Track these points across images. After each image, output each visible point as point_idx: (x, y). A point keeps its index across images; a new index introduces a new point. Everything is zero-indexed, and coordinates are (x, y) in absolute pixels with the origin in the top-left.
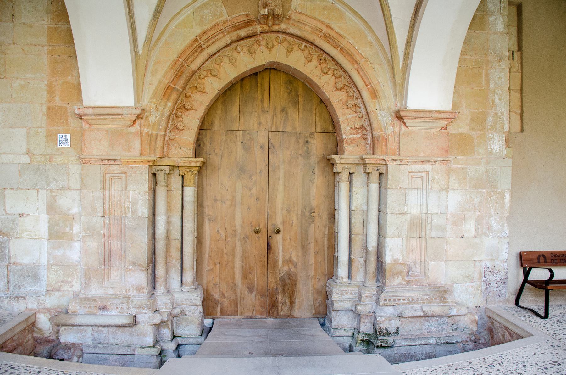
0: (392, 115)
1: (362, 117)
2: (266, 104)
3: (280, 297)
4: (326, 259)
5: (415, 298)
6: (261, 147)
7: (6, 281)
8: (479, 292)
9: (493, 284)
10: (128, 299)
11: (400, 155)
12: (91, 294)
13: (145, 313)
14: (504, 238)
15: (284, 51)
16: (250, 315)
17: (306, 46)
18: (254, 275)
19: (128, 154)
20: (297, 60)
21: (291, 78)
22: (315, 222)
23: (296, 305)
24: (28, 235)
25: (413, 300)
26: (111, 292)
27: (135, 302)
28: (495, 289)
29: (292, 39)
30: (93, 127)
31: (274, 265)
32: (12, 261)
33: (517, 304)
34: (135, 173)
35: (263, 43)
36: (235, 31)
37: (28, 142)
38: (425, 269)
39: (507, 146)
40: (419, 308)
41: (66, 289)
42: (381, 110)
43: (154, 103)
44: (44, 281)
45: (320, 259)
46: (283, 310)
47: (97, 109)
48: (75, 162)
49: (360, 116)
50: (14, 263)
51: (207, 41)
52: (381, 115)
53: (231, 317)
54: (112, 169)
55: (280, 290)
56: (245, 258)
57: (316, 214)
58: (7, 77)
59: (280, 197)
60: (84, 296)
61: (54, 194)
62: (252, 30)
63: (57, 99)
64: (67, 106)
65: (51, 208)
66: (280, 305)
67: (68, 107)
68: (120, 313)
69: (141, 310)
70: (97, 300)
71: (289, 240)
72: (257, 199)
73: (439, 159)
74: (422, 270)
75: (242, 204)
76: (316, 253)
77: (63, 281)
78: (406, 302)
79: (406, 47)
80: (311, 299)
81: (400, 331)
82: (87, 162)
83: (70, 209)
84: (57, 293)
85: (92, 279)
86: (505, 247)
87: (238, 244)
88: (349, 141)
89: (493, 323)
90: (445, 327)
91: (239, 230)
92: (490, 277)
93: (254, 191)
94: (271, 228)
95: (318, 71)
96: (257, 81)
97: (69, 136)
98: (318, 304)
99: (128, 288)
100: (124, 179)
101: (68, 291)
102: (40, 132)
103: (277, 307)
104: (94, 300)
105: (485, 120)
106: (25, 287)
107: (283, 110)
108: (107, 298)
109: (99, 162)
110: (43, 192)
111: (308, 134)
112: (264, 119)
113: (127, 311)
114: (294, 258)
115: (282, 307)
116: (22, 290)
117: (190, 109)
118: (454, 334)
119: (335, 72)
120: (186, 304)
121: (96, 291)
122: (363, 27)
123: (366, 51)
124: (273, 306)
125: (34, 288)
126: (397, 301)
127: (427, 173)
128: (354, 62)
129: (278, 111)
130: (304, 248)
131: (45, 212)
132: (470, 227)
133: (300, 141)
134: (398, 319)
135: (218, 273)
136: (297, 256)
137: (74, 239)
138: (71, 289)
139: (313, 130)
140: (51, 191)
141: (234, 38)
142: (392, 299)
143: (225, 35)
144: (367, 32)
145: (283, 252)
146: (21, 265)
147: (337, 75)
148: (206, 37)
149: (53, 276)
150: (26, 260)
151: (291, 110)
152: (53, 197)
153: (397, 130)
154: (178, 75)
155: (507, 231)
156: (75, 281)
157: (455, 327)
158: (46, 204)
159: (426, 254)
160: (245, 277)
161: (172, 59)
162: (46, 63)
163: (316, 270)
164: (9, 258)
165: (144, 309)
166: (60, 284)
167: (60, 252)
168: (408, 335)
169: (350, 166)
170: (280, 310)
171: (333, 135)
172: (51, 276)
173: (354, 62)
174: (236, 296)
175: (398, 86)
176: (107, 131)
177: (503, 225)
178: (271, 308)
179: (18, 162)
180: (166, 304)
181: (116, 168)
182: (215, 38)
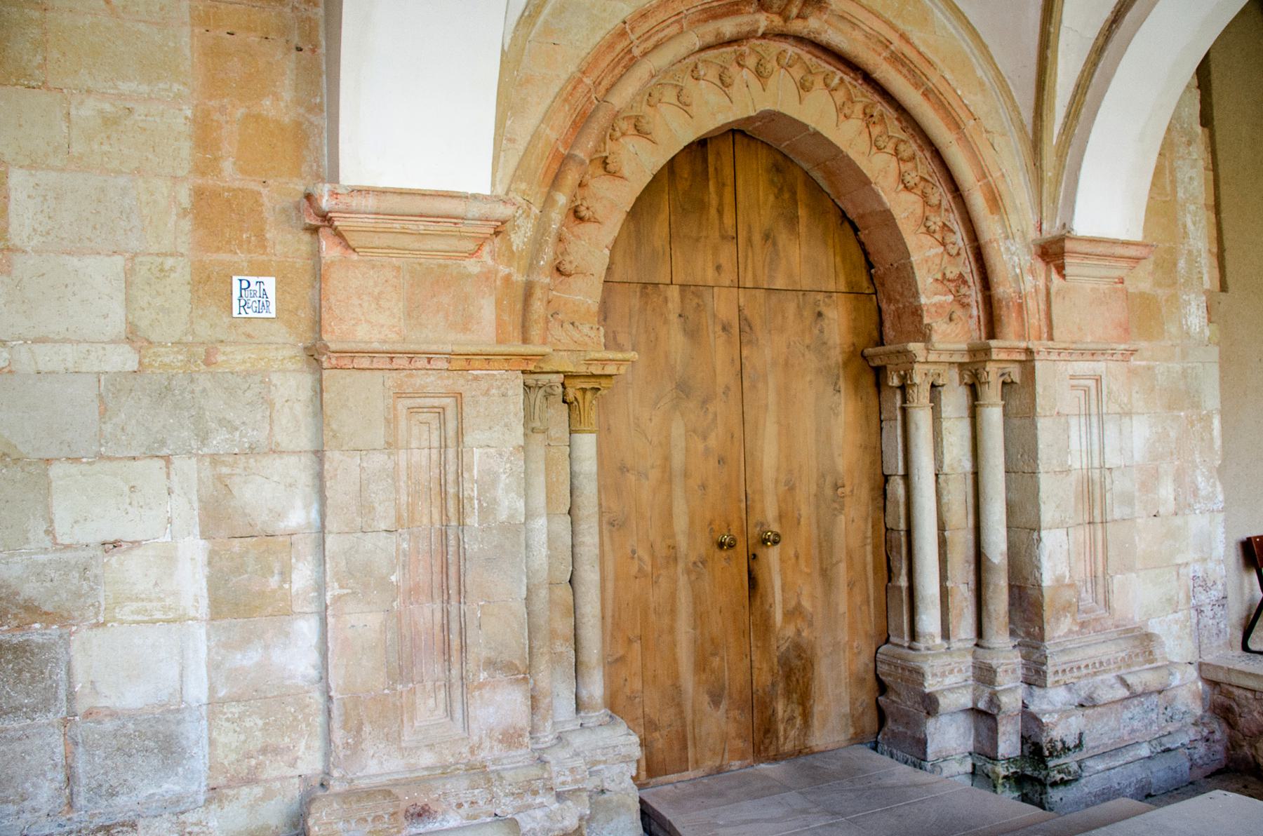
0: (1029, 248)
1: (958, 254)
2: (728, 220)
3: (780, 707)
4: (872, 598)
5: (1104, 659)
6: (724, 329)
7: (61, 777)
8: (1188, 630)
9: (1207, 609)
10: (479, 773)
11: (1051, 338)
12: (369, 777)
13: (542, 805)
14: (1219, 511)
15: (792, 87)
16: (717, 764)
17: (842, 80)
18: (722, 659)
19: (462, 337)
20: (828, 113)
21: (779, 157)
22: (846, 509)
23: (816, 722)
24: (138, 612)
25: (1101, 663)
26: (427, 759)
27: (509, 776)
28: (1211, 622)
29: (814, 59)
30: (355, 257)
31: (764, 626)
32: (81, 707)
33: (1245, 648)
34: (487, 393)
35: (751, 61)
36: (706, 21)
37: (128, 301)
38: (1107, 592)
39: (1210, 321)
40: (1113, 681)
41: (275, 774)
42: (1007, 238)
43: (524, 192)
44: (199, 760)
45: (858, 599)
46: (788, 739)
47: (390, 197)
48: (290, 366)
49: (954, 252)
50: (89, 714)
51: (646, 40)
52: (1008, 249)
53: (673, 777)
54: (418, 382)
55: (781, 686)
56: (699, 618)
57: (847, 489)
58: (51, 85)
59: (769, 455)
60: (346, 787)
61: (225, 470)
62: (748, 24)
63: (228, 166)
64: (262, 190)
65: (217, 516)
66: (781, 727)
67: (265, 191)
68: (468, 818)
69: (529, 799)
70: (395, 791)
71: (793, 560)
72: (721, 461)
73: (1122, 347)
74: (1101, 597)
75: (686, 475)
76: (851, 585)
77: (264, 751)
78: (1090, 670)
79: (1074, 96)
80: (846, 699)
81: (1086, 740)
82: (342, 363)
83: (280, 515)
84: (245, 790)
85: (367, 728)
86: (1220, 530)
87: (683, 580)
88: (933, 310)
89: (1231, 693)
90: (1154, 716)
91: (682, 542)
92: (1203, 597)
93: (712, 442)
94: (754, 531)
95: (863, 143)
96: (705, 160)
97: (270, 283)
98: (860, 710)
99: (476, 738)
100: (450, 414)
101: (283, 779)
102: (172, 269)
103: (776, 731)
104: (386, 793)
105: (1175, 265)
106: (132, 789)
107: (767, 237)
108: (418, 782)
109: (381, 362)
110: (186, 467)
111: (820, 296)
112: (727, 254)
113: (489, 808)
114: (806, 604)
115: (785, 730)
116: (121, 800)
117: (589, 220)
118: (1169, 729)
119: (902, 147)
120: (605, 762)
121: (379, 764)
122: (965, 44)
123: (973, 99)
124: (767, 731)
125: (166, 786)
126: (1076, 673)
127: (1098, 380)
128: (956, 125)
129: (757, 238)
130: (826, 574)
131: (197, 530)
132: (1167, 491)
133: (805, 314)
134: (1080, 712)
135: (637, 665)
136: (813, 597)
137: (297, 609)
138: (290, 772)
139: (832, 287)
140: (215, 459)
141: (710, 39)
142: (1067, 667)
143: (681, 32)
144: (976, 60)
145: (783, 591)
146: (113, 714)
147: (905, 155)
148: (646, 27)
149: (228, 738)
150: (132, 697)
151: (784, 236)
152: (220, 478)
153: (1041, 283)
154: (581, 122)
155: (1221, 497)
156: (302, 744)
157: (1169, 712)
158: (196, 505)
159: (1106, 558)
160: (701, 665)
161: (564, 77)
162: (187, 52)
163: (852, 628)
164: (71, 697)
165: (535, 793)
166: (253, 762)
167: (248, 659)
168: (1098, 747)
169: (940, 369)
170: (782, 739)
171: (871, 300)
172: (222, 739)
173: (956, 125)
174: (683, 719)
175: (1046, 186)
176: (398, 269)
177: (1214, 486)
178: (762, 739)
179: (96, 369)
180: (572, 770)
181: (430, 381)
182: (661, 35)
